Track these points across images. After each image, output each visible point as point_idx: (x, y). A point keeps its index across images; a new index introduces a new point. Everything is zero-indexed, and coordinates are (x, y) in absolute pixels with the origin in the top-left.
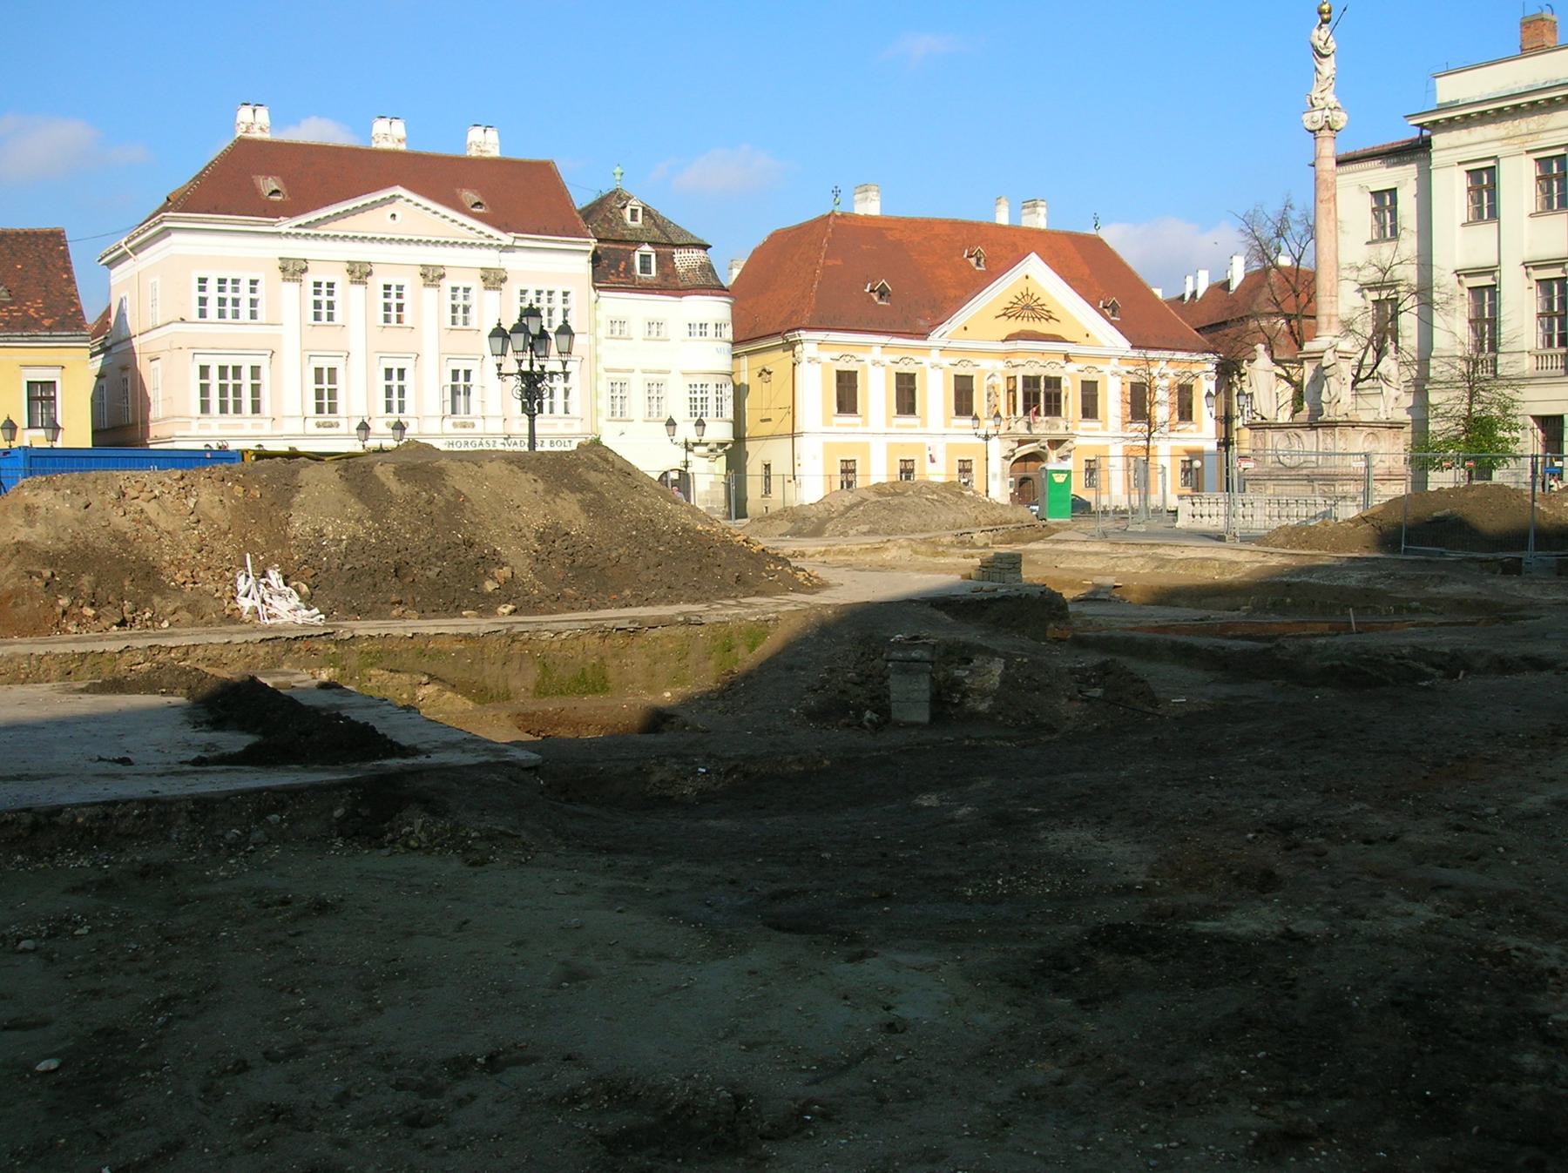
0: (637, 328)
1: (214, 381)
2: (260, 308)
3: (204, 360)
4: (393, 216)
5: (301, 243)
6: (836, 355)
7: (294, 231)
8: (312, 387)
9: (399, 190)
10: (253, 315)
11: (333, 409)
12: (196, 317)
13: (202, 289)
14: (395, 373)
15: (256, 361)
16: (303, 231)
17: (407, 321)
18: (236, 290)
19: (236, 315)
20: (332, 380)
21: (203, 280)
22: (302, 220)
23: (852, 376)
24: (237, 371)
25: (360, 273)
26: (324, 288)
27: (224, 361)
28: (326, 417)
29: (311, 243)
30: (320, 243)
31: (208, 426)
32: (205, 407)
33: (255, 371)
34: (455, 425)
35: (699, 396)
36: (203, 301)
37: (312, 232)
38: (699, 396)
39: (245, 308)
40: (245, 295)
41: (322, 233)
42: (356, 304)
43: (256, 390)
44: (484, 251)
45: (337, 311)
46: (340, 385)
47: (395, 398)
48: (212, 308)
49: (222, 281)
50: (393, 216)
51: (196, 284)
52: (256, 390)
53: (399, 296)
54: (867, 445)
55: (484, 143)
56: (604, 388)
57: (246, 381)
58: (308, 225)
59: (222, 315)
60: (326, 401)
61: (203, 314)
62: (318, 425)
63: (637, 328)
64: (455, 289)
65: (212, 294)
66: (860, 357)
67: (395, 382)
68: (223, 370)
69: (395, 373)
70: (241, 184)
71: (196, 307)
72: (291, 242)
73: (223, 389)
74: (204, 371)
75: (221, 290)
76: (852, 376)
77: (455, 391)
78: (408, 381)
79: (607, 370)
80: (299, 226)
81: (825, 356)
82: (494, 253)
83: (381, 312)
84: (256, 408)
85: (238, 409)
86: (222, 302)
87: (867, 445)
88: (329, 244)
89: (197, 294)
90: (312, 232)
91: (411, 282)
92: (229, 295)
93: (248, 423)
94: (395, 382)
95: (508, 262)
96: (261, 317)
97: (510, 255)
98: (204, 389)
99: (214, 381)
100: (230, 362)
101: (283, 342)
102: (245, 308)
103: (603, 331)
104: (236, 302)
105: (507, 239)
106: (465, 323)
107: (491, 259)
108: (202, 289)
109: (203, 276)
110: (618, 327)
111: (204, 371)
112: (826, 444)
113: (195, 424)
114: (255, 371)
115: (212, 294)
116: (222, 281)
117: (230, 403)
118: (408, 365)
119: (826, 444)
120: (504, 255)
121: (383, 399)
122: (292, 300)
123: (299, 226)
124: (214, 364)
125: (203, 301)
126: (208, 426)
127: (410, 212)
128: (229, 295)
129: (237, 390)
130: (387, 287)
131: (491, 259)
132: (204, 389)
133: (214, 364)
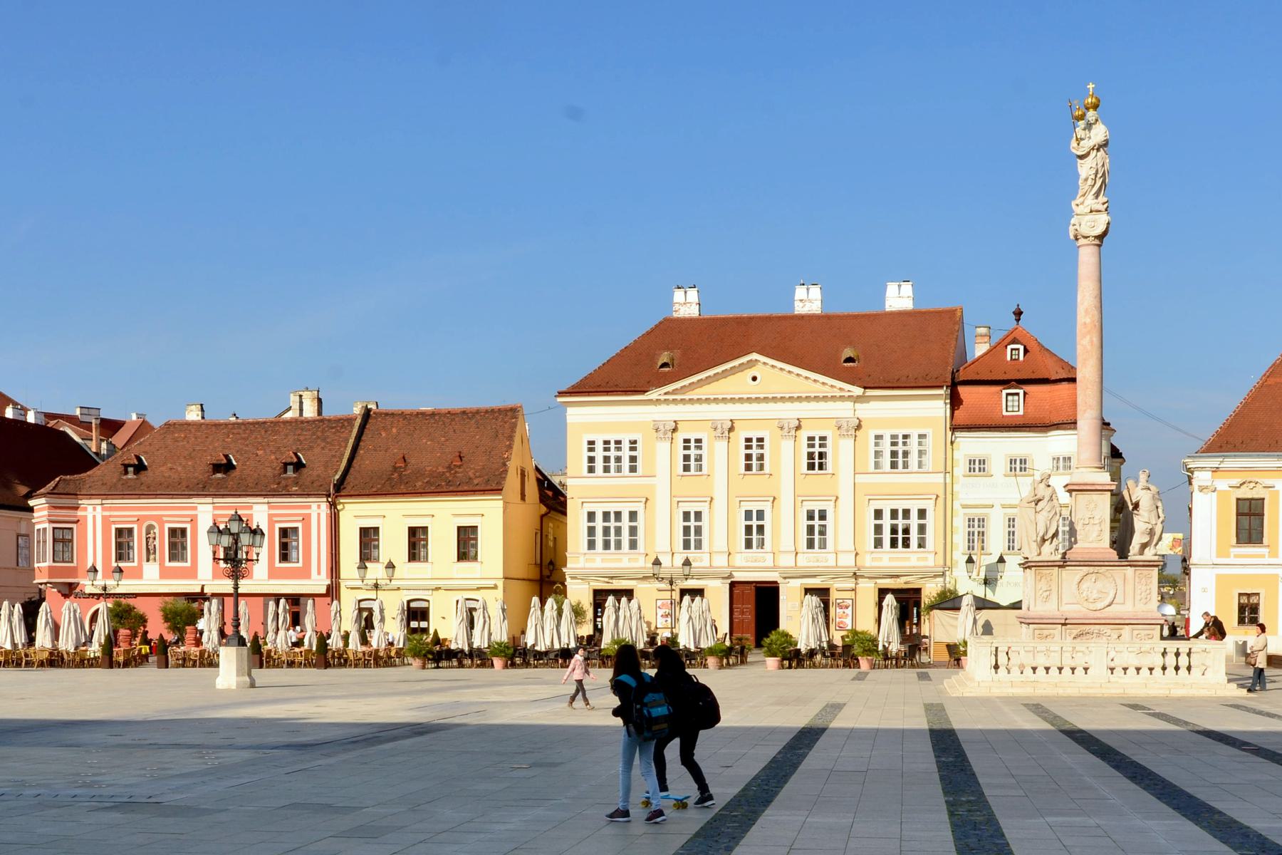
0: (998, 466)
1: (599, 524)
2: (639, 464)
5: (672, 407)
6: (1236, 482)
7: (663, 398)
9: (754, 356)
12: (872, 469)
14: (612, 516)
15: (759, 506)
16: (671, 397)
17: (767, 469)
18: (619, 449)
19: (619, 470)
21: (591, 443)
22: (670, 388)
26: (612, 446)
29: (680, 407)
30: (688, 407)
31: (926, 559)
32: (591, 545)
33: (633, 516)
36: (591, 460)
37: (678, 397)
39: (626, 464)
40: (626, 453)
41: (695, 397)
42: (721, 458)
44: (839, 404)
45: (704, 462)
48: (599, 464)
49: (607, 442)
50: (754, 379)
51: (586, 446)
52: (633, 531)
55: (808, 301)
57: (625, 523)
58: (674, 392)
59: (607, 470)
60: (692, 537)
61: (591, 470)
63: (998, 466)
64: (811, 439)
65: (599, 454)
66: (1269, 482)
68: (606, 516)
69: (612, 516)
70: (653, 361)
71: (585, 464)
72: (663, 408)
73: (606, 531)
74: (878, 514)
75: (606, 449)
78: (829, 522)
79: (965, 507)
81: (1223, 484)
82: (849, 404)
83: (743, 462)
84: (633, 545)
85: (618, 545)
86: (607, 459)
88: (697, 407)
89: (586, 454)
90: (678, 397)
92: (613, 454)
93: (625, 559)
94: (692, 523)
97: (865, 406)
98: (878, 529)
99: (599, 524)
101: (657, 493)
102: (913, 459)
103: (961, 468)
104: (618, 459)
108: (591, 450)
109: (633, 438)
110: (978, 466)
112: (1218, 576)
113: (582, 559)
114: (633, 516)
115: (599, 454)
117: (900, 539)
118: (766, 507)
119: (1218, 576)
120: (858, 405)
121: (743, 537)
122: (661, 458)
124: (599, 510)
125: (591, 460)
126: (594, 561)
127: (770, 374)
128: (613, 454)
129: (618, 531)
130: (748, 440)
131: (844, 410)
132: (591, 531)
133: (599, 510)
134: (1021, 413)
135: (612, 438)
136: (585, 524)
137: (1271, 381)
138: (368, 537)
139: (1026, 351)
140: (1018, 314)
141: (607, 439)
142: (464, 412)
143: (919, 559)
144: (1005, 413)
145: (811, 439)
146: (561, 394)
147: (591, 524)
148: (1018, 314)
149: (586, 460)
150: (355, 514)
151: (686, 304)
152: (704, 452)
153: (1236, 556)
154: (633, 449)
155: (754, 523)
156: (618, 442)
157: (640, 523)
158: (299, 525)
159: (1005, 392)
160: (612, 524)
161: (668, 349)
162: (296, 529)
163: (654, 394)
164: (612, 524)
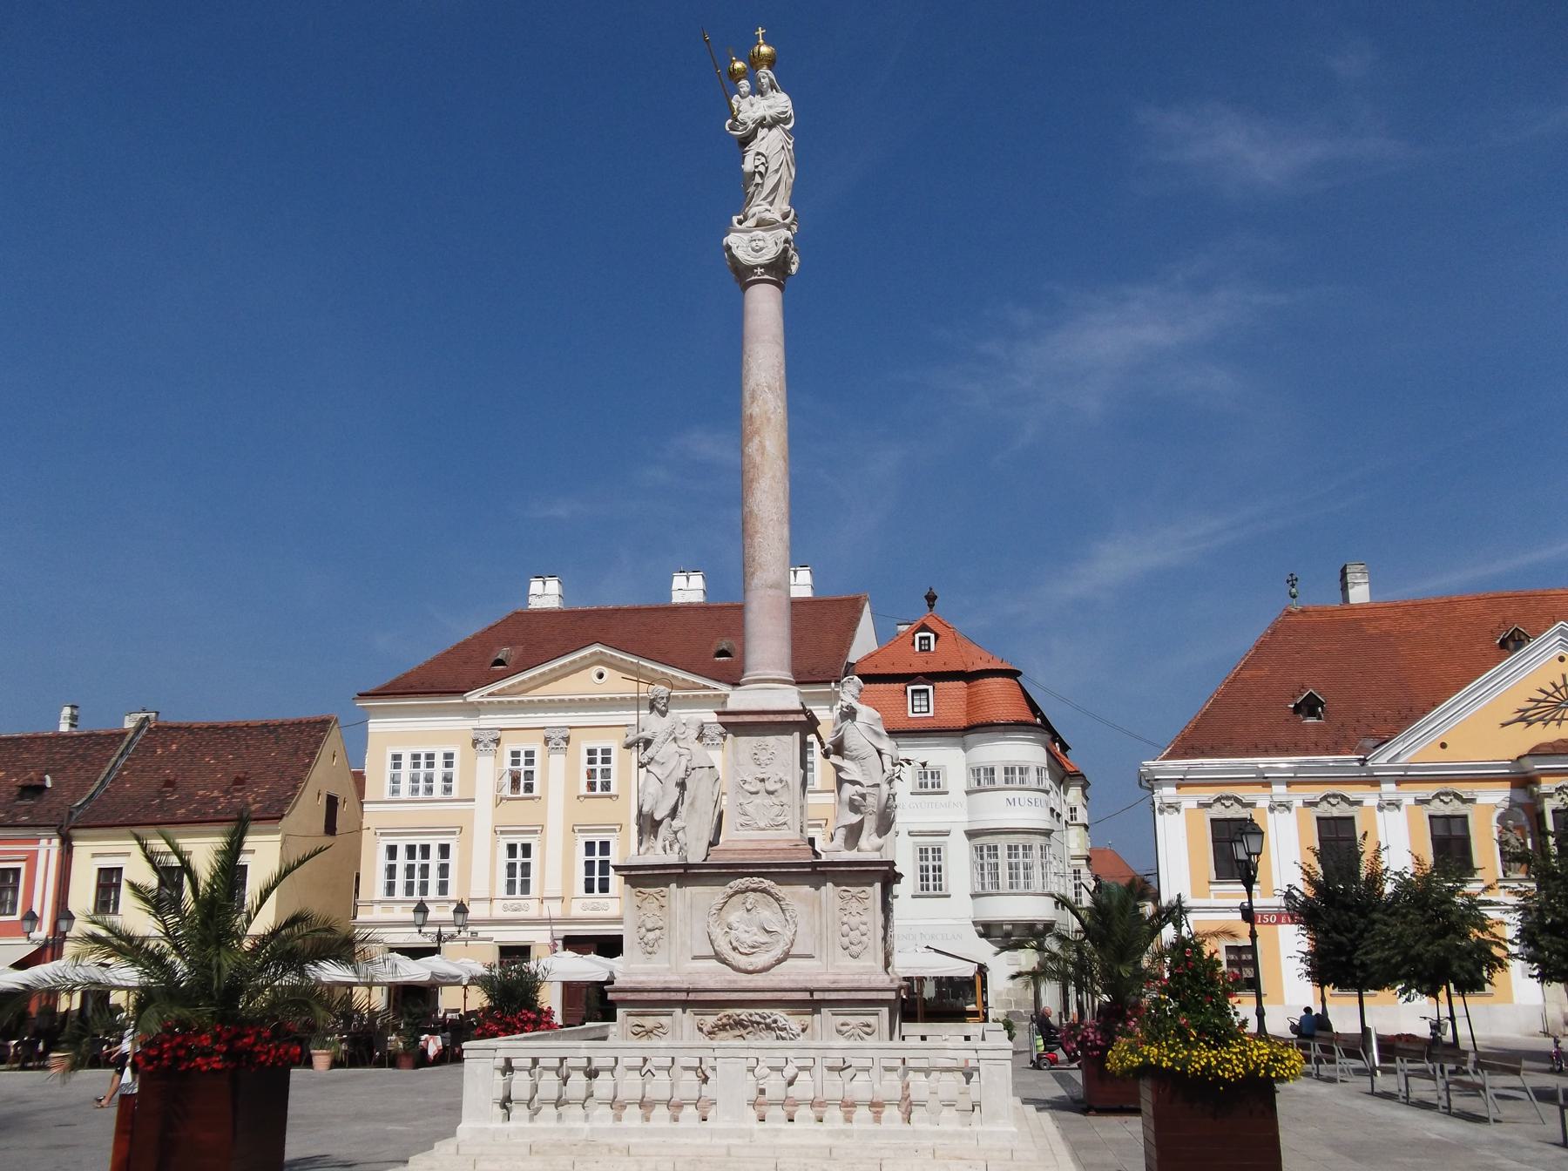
1: (402, 860)
2: (455, 784)
3: (392, 841)
4: (1443, 746)
9: (597, 648)
10: (448, 790)
12: (387, 796)
13: (397, 766)
15: (604, 837)
17: (536, 791)
19: (429, 790)
21: (397, 757)
24: (426, 850)
25: (559, 741)
27: (412, 840)
33: (444, 850)
35: (931, 863)
38: (931, 863)
39: (438, 784)
40: (439, 770)
43: (444, 870)
47: (417, 880)
49: (416, 757)
52: (444, 870)
57: (434, 860)
64: (515, 754)
67: (519, 859)
68: (411, 850)
73: (410, 870)
74: (392, 851)
80: (490, 695)
86: (415, 780)
94: (519, 859)
96: (455, 794)
98: (391, 870)
99: (402, 860)
100: (418, 841)
102: (438, 784)
111: (392, 851)
116: (416, 757)
118: (533, 841)
130: (591, 752)
132: (391, 870)
134: (931, 714)
135: (423, 751)
136: (382, 861)
137: (1246, 674)
138: (109, 881)
139: (937, 637)
140: (931, 599)
141: (516, 749)
142: (265, 726)
143: (505, 908)
144: (910, 714)
145: (515, 754)
146: (363, 695)
147: (444, 861)
148: (931, 599)
149: (388, 779)
150: (90, 856)
151: (545, 594)
152: (536, 768)
153: (1217, 896)
154: (448, 765)
155: (597, 858)
156: (430, 756)
157: (453, 861)
158: (22, 865)
159: (910, 688)
160: (418, 861)
161: (509, 644)
162: (17, 871)
163: (474, 697)
164: (418, 861)
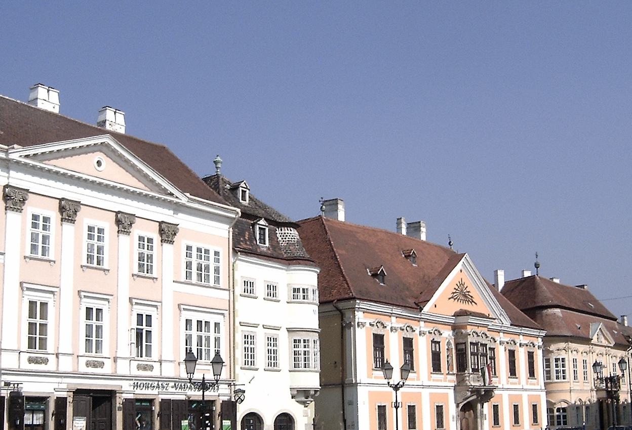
8: (25, 320)
11: (43, 345)
20: (149, 324)
23: (382, 337)
28: (37, 353)
34: (139, 367)
46: (154, 329)
53: (45, 228)
54: (420, 393)
56: (240, 339)
62: (31, 360)
76: (382, 337)
77: (139, 334)
80: (27, 156)
87: (420, 393)
91: (108, 224)
95: (183, 220)
103: (239, 289)
105: (183, 199)
106: (99, 263)
107: (166, 215)
112: (431, 394)
123: (27, 156)
131: (166, 215)
